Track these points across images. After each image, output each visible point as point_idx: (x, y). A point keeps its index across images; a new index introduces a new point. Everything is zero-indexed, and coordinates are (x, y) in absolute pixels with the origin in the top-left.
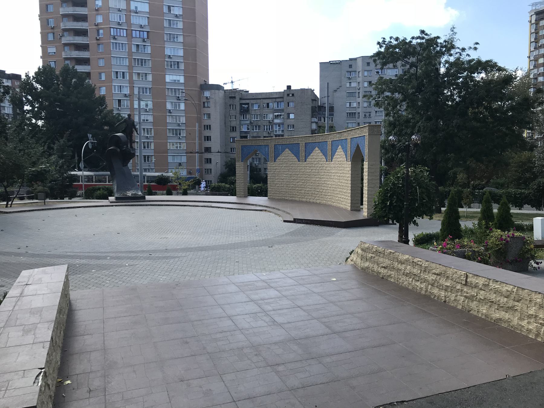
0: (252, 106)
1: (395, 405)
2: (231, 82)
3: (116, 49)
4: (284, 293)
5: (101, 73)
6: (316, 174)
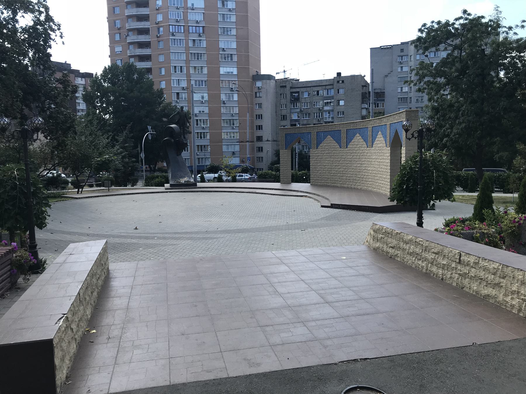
0: (302, 94)
1: (358, 361)
2: (283, 71)
3: (175, 45)
4: (293, 269)
5: (161, 68)
6: (357, 160)
